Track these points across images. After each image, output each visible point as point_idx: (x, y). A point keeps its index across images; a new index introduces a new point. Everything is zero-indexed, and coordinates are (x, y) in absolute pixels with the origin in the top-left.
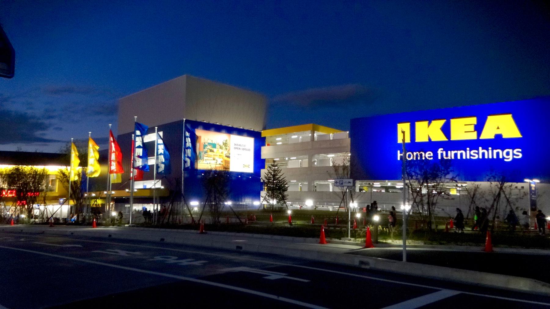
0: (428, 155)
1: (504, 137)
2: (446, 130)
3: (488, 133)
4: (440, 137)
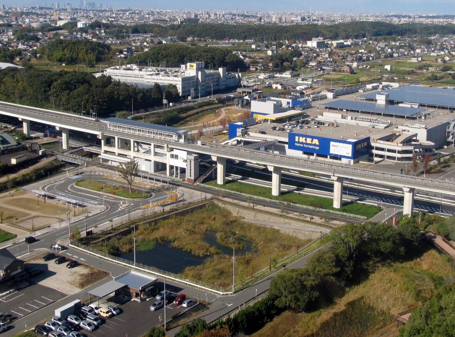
0: (302, 145)
1: (302, 152)
2: (306, 140)
3: (313, 143)
4: (304, 141)
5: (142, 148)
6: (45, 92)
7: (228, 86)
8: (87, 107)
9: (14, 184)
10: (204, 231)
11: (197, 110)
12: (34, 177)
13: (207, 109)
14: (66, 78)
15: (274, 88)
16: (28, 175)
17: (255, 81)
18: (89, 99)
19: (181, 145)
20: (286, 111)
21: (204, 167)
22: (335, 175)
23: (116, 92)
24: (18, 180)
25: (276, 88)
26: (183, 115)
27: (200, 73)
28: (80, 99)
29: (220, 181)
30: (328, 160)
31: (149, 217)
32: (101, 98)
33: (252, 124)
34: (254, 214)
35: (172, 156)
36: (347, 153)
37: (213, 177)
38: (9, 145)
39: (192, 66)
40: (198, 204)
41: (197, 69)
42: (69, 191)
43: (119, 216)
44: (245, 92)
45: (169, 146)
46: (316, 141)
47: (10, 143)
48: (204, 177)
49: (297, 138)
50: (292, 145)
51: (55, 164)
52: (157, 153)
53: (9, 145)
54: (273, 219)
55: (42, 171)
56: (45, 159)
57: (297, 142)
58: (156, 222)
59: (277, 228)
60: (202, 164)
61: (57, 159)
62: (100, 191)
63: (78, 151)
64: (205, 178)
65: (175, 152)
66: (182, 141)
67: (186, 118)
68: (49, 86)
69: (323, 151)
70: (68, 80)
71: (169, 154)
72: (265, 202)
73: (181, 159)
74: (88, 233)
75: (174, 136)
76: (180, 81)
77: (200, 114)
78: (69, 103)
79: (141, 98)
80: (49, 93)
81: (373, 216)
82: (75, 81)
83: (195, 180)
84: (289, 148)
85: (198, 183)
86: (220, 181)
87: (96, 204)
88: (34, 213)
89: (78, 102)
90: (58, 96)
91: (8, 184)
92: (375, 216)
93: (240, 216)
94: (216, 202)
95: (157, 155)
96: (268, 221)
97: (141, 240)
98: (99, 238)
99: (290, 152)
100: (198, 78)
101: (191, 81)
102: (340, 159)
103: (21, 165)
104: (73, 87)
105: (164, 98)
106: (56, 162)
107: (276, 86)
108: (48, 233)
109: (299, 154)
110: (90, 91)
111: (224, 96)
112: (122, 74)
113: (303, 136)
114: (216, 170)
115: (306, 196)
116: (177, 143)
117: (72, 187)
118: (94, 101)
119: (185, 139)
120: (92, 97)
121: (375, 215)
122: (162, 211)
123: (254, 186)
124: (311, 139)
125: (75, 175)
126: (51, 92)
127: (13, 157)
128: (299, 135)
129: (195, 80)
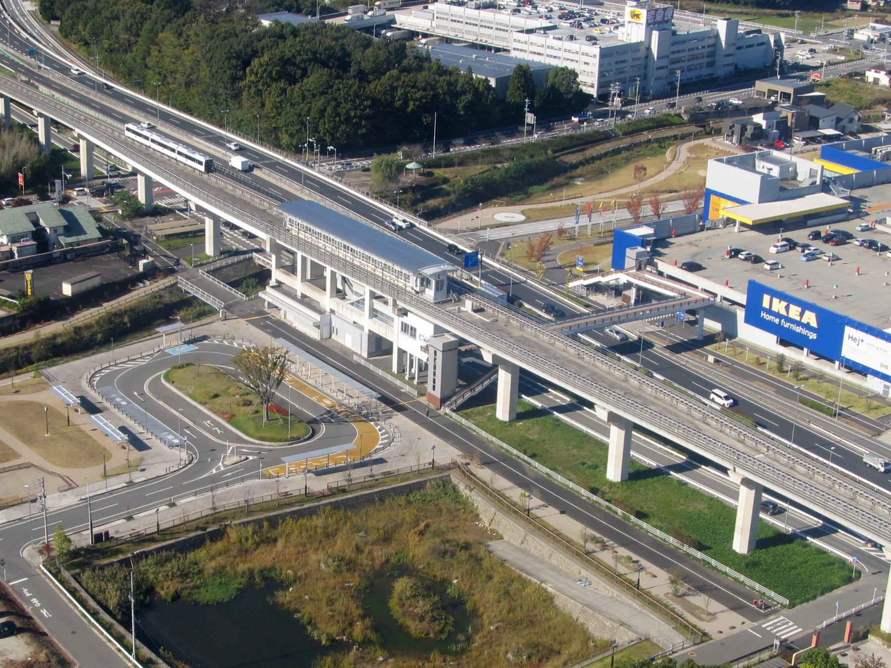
0: (777, 321)
3: (804, 321)
4: (783, 312)
5: (352, 291)
6: (234, 79)
7: (740, 66)
8: (321, 128)
9: (48, 350)
10: (378, 563)
11: (619, 142)
12: (99, 336)
13: (649, 141)
14: (287, 48)
15: (871, 80)
16: (88, 327)
17: (834, 51)
18: (325, 110)
19: (423, 305)
20: (802, 196)
21: (468, 373)
22: (737, 469)
23: (400, 92)
24: (59, 340)
25: (876, 81)
26: (572, 159)
27: (655, 35)
28: (306, 109)
29: (502, 410)
30: (833, 370)
31: (264, 507)
32: (356, 108)
33: (686, 231)
34: (523, 534)
35: (405, 328)
36: (882, 365)
37: (489, 396)
38: (82, 237)
39: (638, 16)
40: (408, 479)
41: (648, 24)
42: (142, 394)
43: (196, 494)
44: (777, 92)
45: (398, 302)
46: (810, 318)
47: (85, 233)
48: (468, 395)
49: (766, 298)
50: (754, 317)
51: (167, 299)
52: (376, 311)
53: (82, 237)
54: (560, 558)
55: (126, 319)
56: (148, 283)
57: (765, 310)
58: (273, 522)
59: (550, 589)
60: (465, 360)
61: (176, 284)
62: (204, 404)
63: (239, 262)
64: (471, 398)
65: (410, 320)
66: (430, 294)
67: (575, 166)
68: (247, 63)
69: (827, 343)
70: (288, 54)
71: (398, 320)
72: (574, 497)
73: (418, 337)
74: (98, 538)
75: (413, 278)
76: (595, 56)
77: (624, 154)
78: (280, 114)
79: (468, 107)
80: (242, 84)
81: (814, 597)
82: (305, 57)
83: (443, 401)
84: (747, 320)
85: (448, 411)
86: (502, 410)
87: (172, 446)
88: (28, 454)
89: (300, 115)
90: (259, 93)
91: (34, 351)
92: (820, 599)
93: (492, 531)
94: (455, 478)
95: (376, 316)
96: (547, 559)
97: (211, 571)
98: (117, 552)
99: (747, 333)
100: (649, 49)
101: (629, 57)
102: (865, 375)
103: (86, 299)
104: (299, 72)
105: (526, 109)
106: (171, 293)
107: (877, 75)
108: (20, 519)
109: (767, 341)
110: (331, 87)
111: (711, 99)
112: (470, 18)
113: (782, 296)
114: (495, 384)
115: (696, 493)
116: (416, 299)
117: (155, 385)
118: (338, 115)
119: (437, 289)
120: (333, 103)
121: (822, 594)
122: (303, 492)
123: (586, 436)
124: (800, 309)
125: (185, 343)
126: (244, 83)
127: (65, 279)
128: (774, 294)
129: (642, 53)
